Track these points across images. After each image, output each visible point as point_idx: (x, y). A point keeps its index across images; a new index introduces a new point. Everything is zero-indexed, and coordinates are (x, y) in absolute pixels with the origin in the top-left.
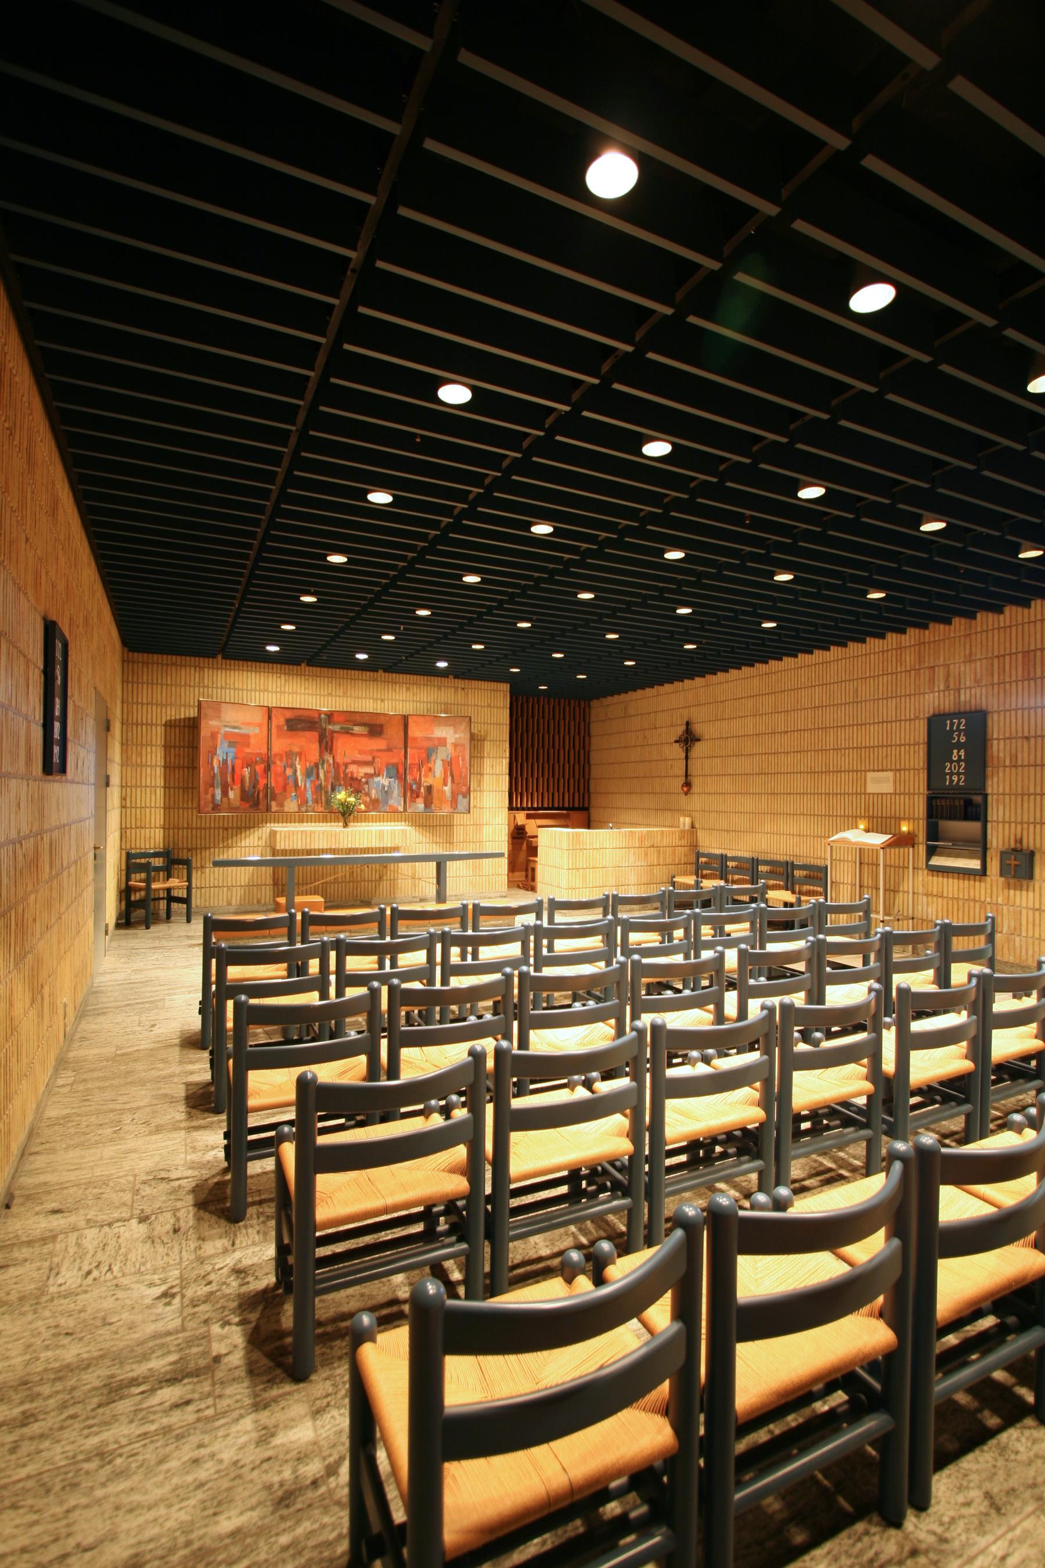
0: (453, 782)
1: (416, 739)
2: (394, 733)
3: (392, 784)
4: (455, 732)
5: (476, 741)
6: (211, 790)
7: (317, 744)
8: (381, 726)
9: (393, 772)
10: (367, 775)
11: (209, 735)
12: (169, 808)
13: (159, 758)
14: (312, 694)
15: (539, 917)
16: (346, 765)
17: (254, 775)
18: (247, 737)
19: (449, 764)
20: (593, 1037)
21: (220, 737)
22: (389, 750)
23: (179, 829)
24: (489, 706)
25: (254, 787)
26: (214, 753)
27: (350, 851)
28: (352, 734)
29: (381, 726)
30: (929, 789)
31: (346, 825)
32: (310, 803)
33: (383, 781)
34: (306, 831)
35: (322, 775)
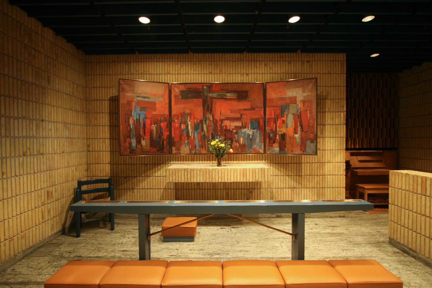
0: (302, 130)
1: (272, 100)
3: (255, 133)
4: (304, 92)
5: (320, 101)
6: (128, 139)
7: (202, 107)
8: (246, 92)
11: (126, 102)
12: (113, 152)
13: (106, 121)
14: (199, 74)
16: (222, 121)
17: (159, 129)
18: (154, 104)
19: (298, 117)
21: (134, 104)
22: (252, 109)
23: (119, 164)
24: (329, 73)
25: (160, 137)
28: (226, 99)
29: (246, 92)
31: (219, 164)
32: (198, 148)
33: (249, 131)
34: (187, 169)
35: (205, 129)
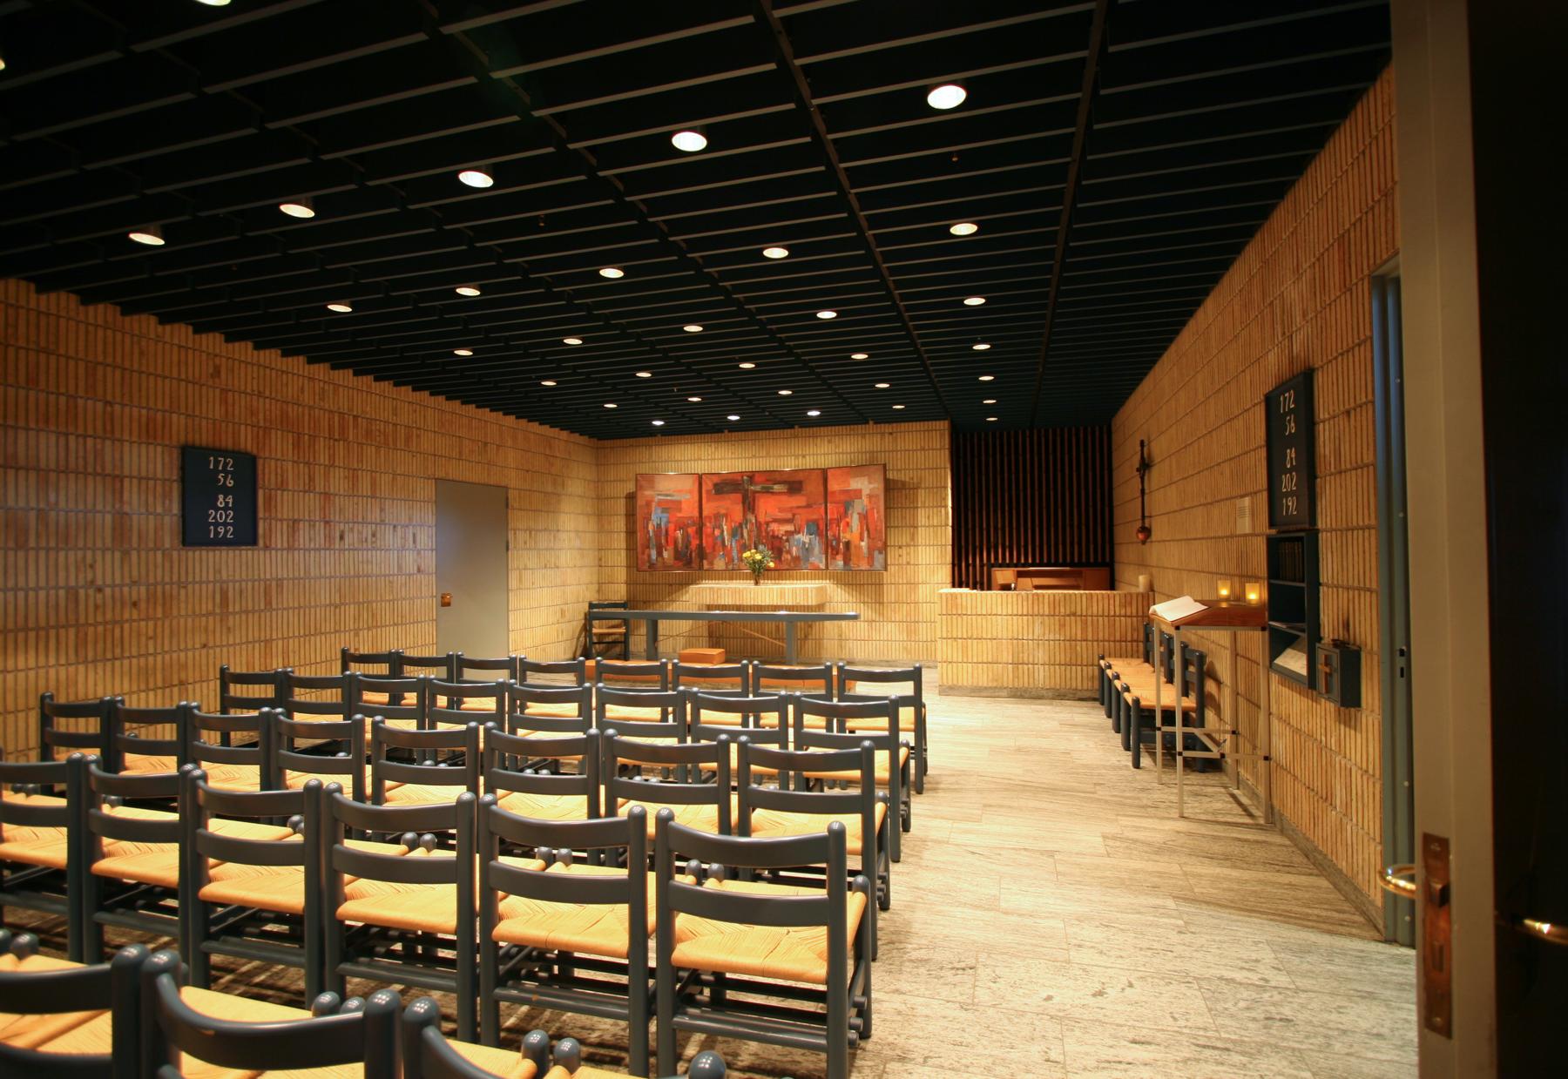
2: (813, 487)
9: (814, 528)
10: (787, 533)
15: (513, 676)
16: (767, 524)
17: (686, 536)
19: (864, 518)
20: (569, 810)
22: (809, 506)
24: (923, 449)
26: (648, 518)
27: (752, 607)
30: (1272, 525)
31: (757, 583)
33: (804, 538)
